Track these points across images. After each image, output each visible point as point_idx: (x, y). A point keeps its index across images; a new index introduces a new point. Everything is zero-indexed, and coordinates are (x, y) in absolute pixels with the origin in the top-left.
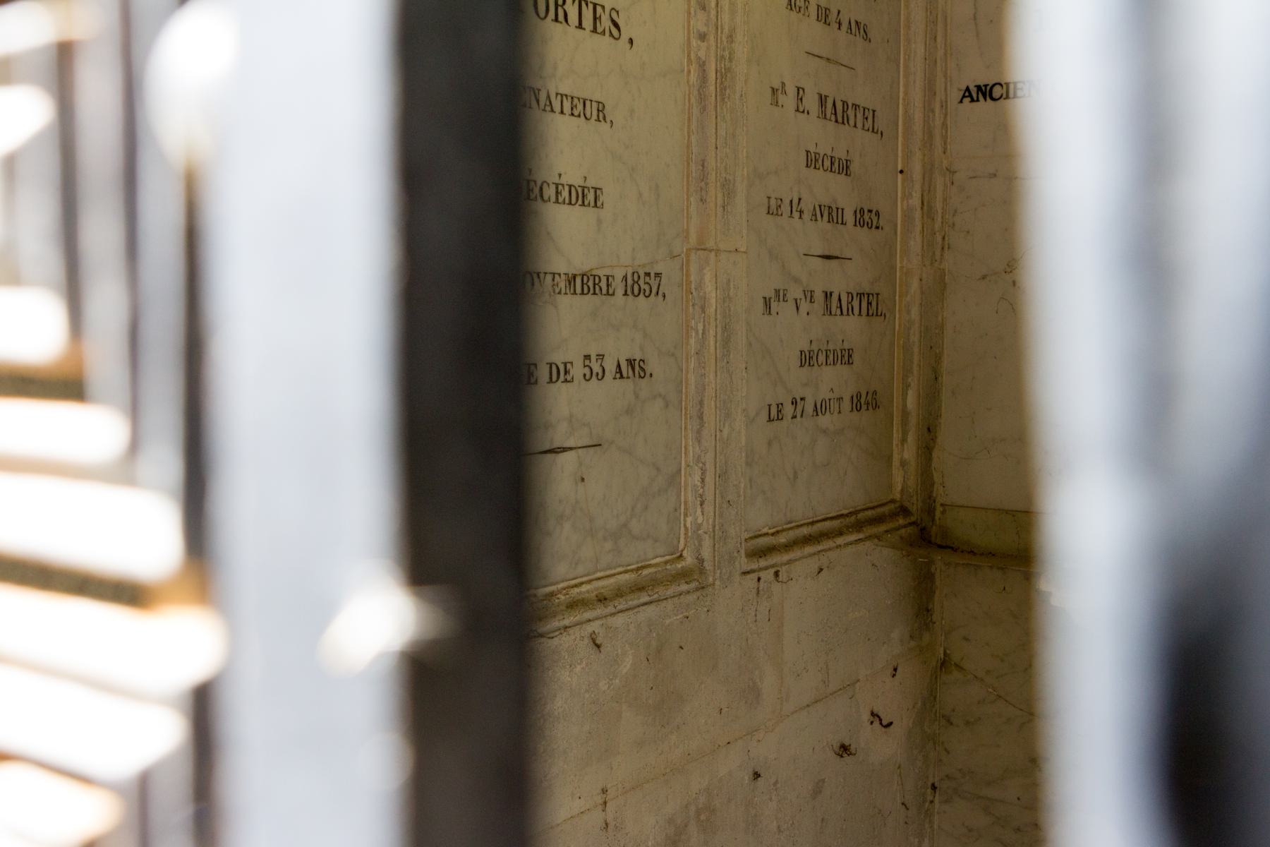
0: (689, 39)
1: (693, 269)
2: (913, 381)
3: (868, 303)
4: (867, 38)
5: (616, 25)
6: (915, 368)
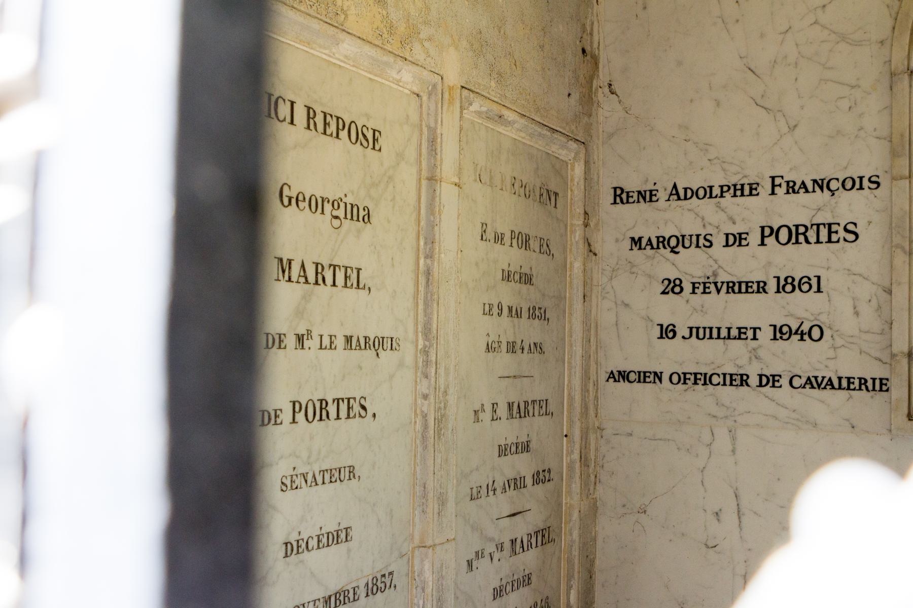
0: (416, 400)
1: (417, 562)
2: (575, 583)
3: (544, 536)
4: (542, 352)
5: (364, 408)
6: (576, 576)
